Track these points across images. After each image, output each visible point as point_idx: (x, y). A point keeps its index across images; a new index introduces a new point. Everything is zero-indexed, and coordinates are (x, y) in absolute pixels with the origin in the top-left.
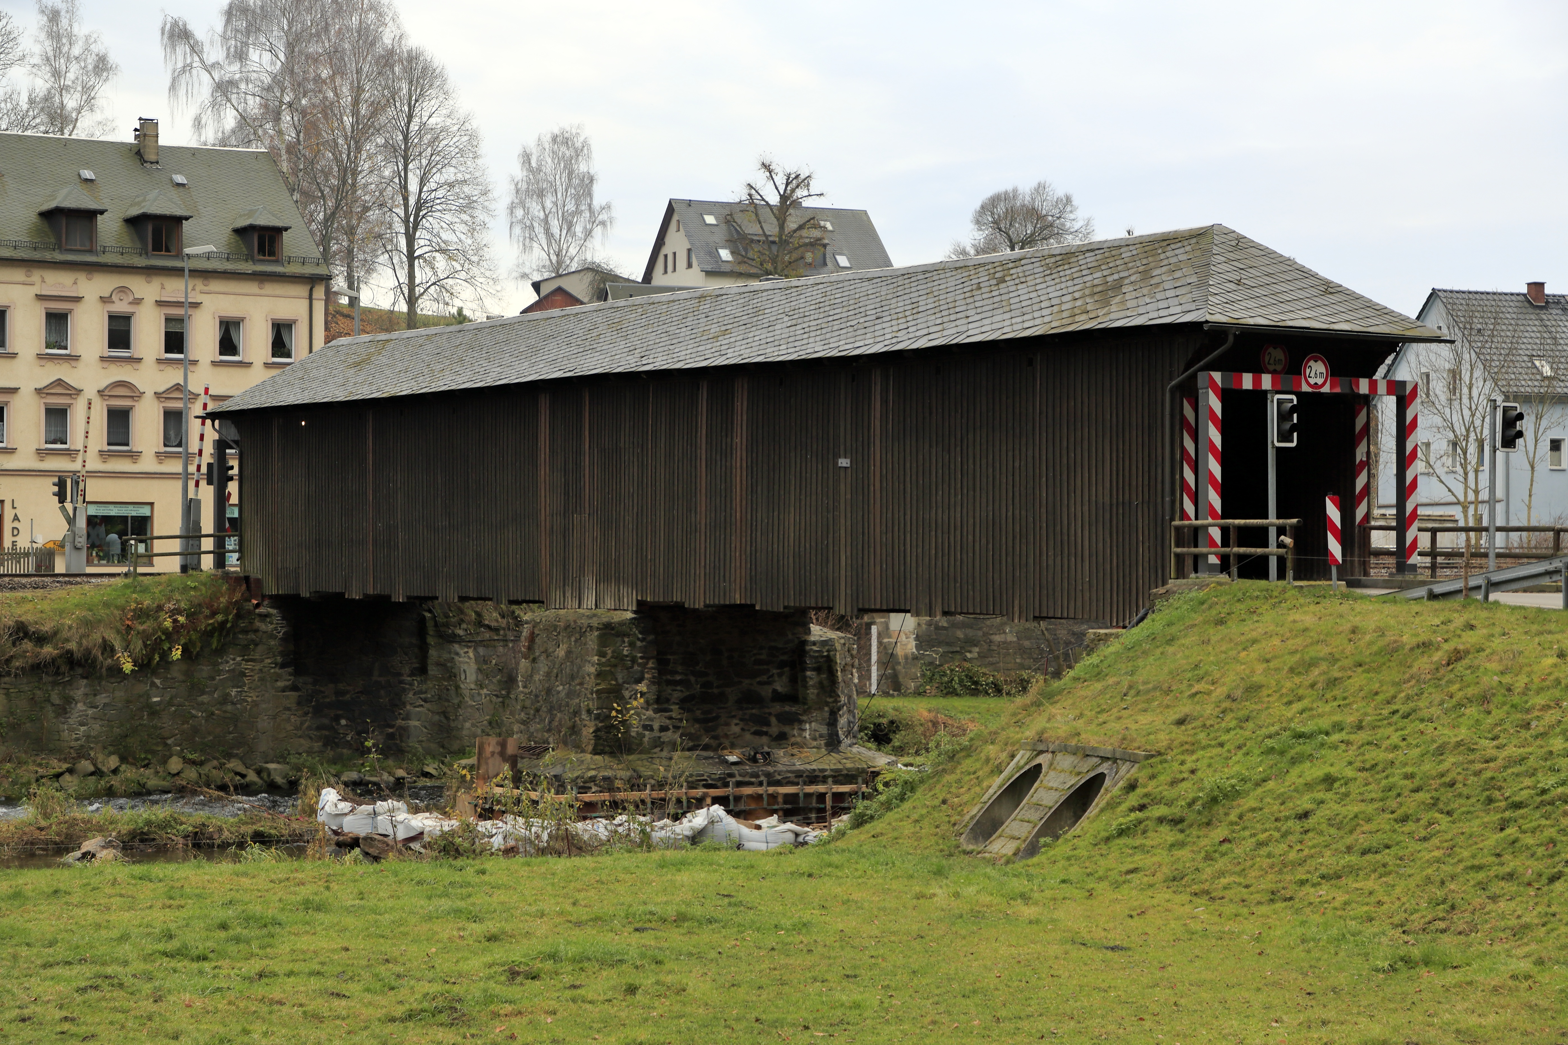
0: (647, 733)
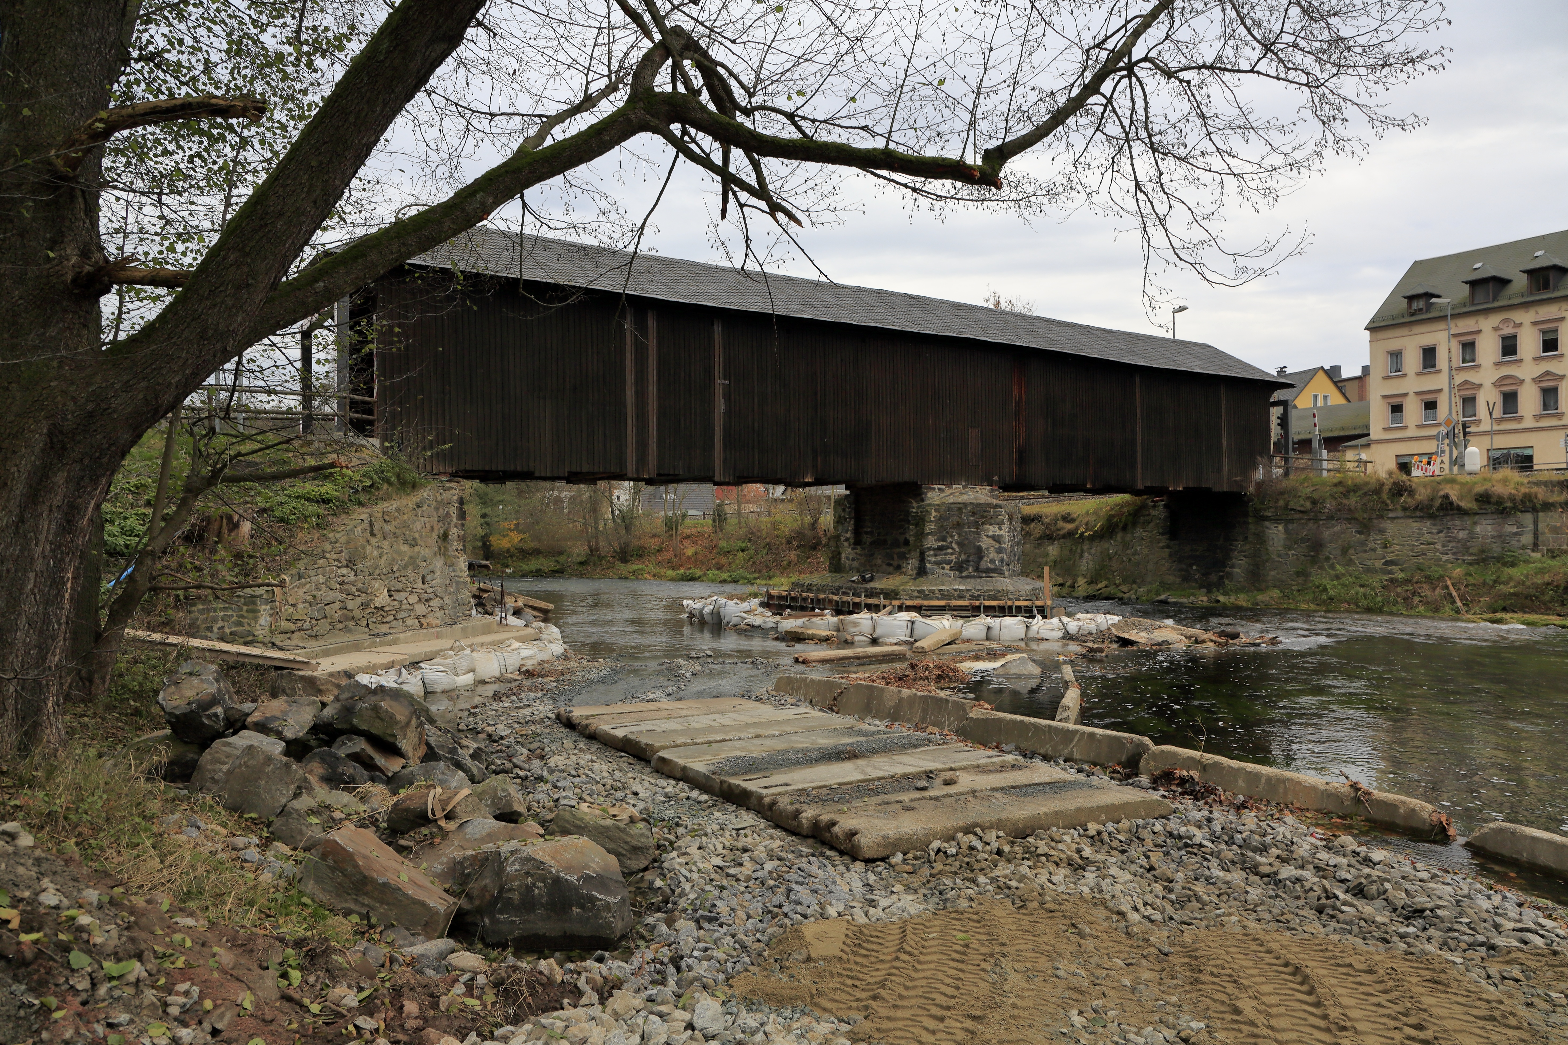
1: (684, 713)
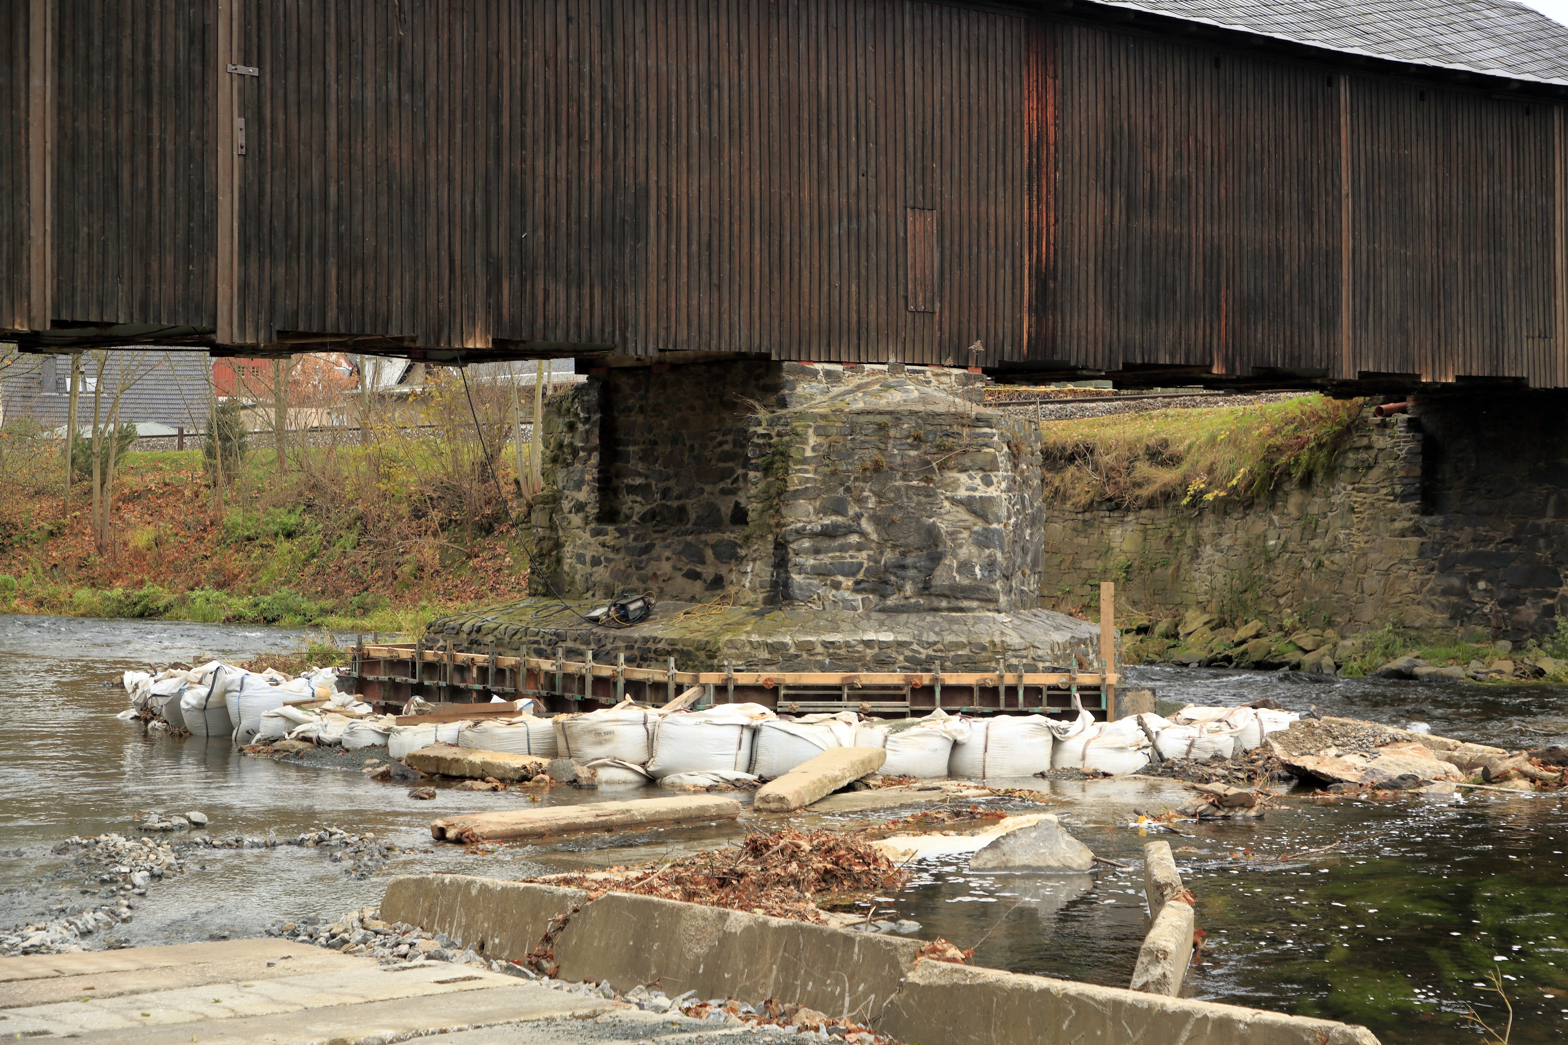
0: (579, 566)
1: (129, 983)
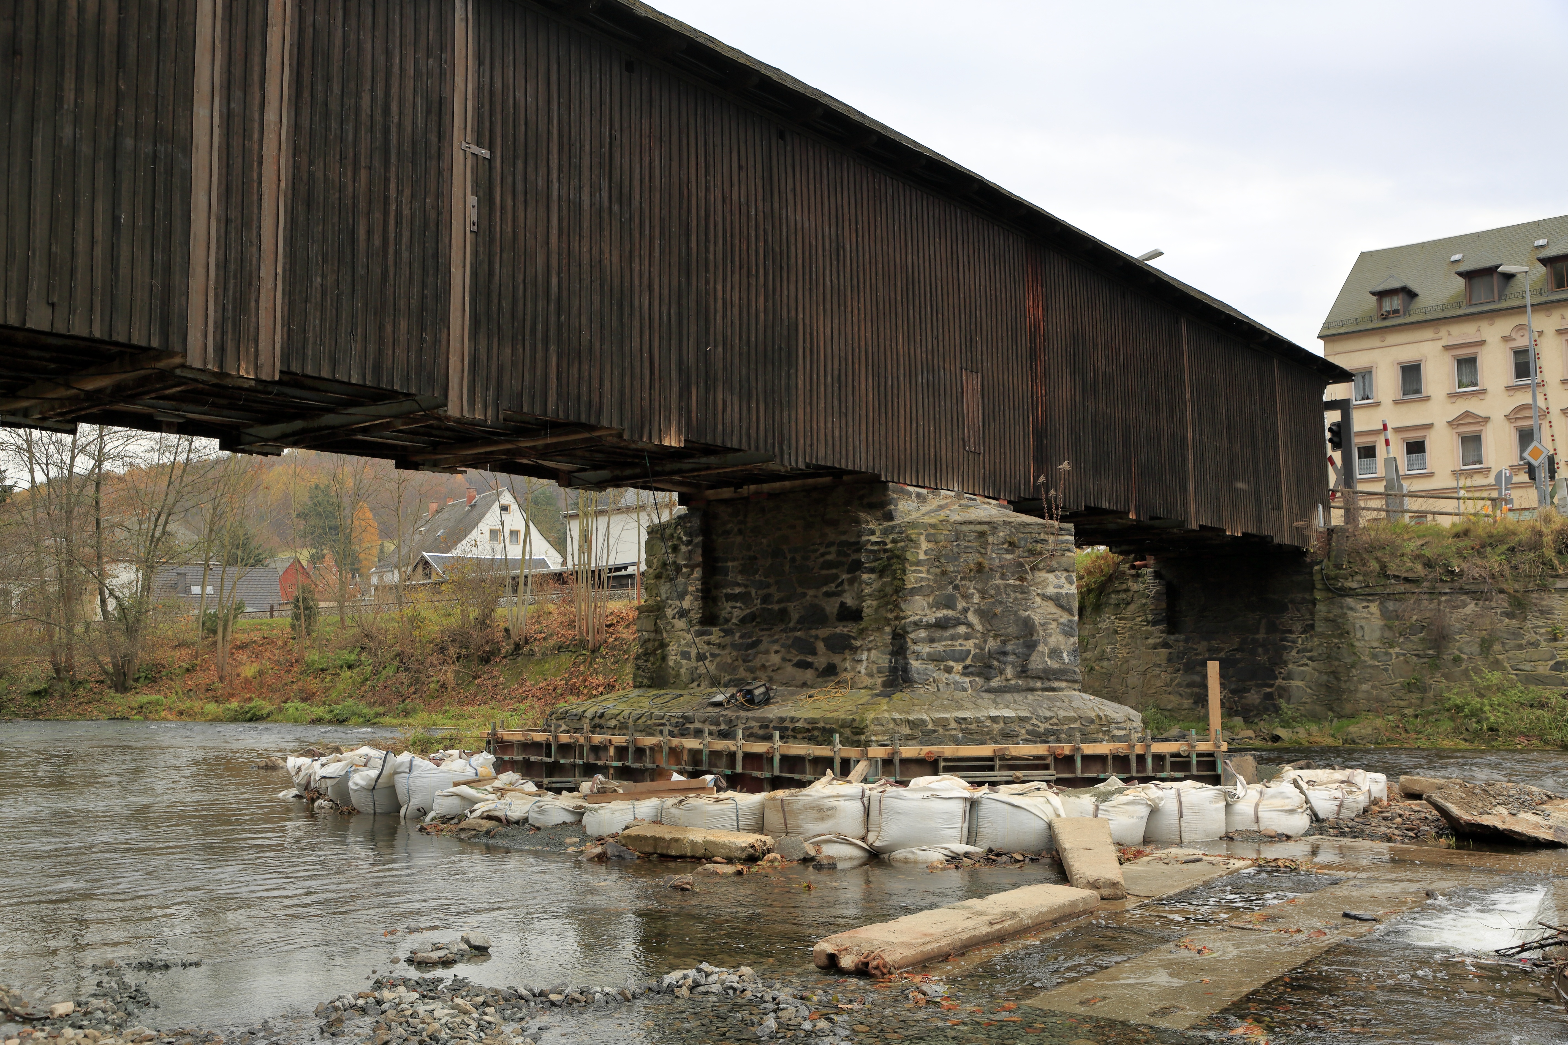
0: (684, 662)
